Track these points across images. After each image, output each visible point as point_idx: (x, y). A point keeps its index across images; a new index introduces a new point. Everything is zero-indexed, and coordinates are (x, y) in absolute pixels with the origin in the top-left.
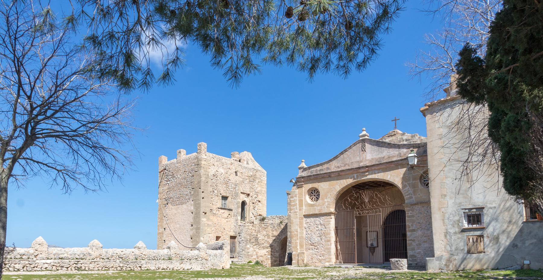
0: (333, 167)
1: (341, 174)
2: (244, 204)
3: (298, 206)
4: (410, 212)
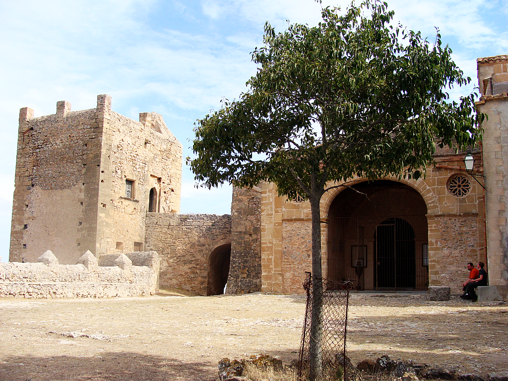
2: (153, 192)
3: (274, 207)
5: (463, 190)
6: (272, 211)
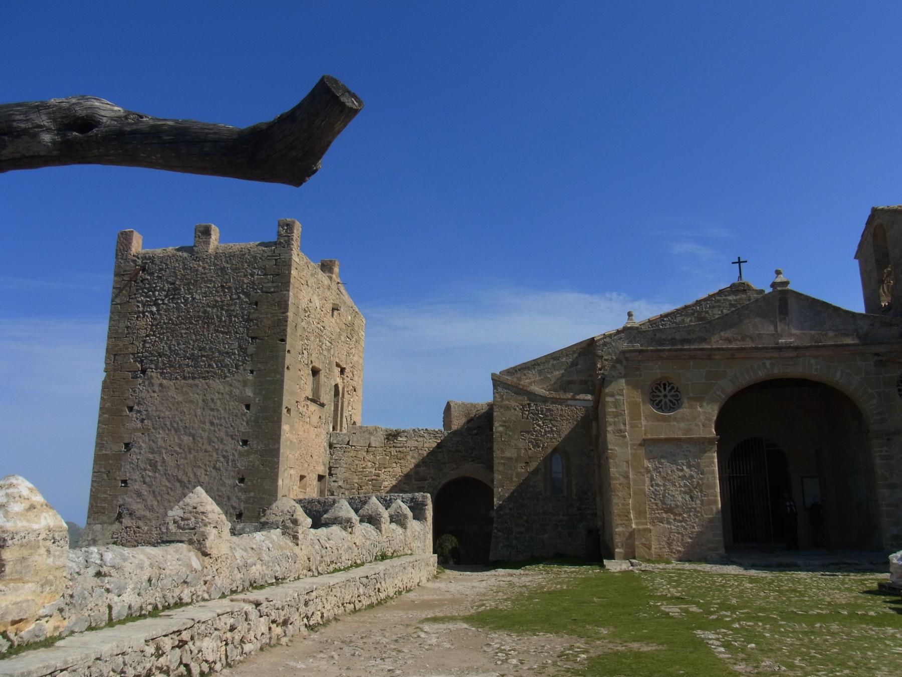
3: (627, 418)
4: (886, 448)
6: (625, 424)
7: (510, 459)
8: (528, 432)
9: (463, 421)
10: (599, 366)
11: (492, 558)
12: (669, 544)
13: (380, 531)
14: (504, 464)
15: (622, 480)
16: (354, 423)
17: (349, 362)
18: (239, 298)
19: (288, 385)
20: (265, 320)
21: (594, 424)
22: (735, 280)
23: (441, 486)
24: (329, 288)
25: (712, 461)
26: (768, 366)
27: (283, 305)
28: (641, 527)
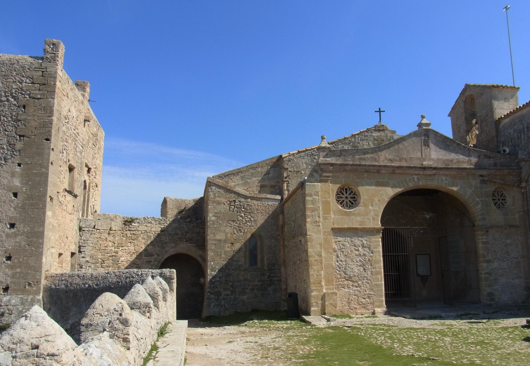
0: (382, 158)
1: (397, 171)
3: (321, 213)
4: (485, 237)
5: (343, 201)
6: (319, 217)
7: (220, 241)
8: (233, 221)
9: (176, 212)
10: (285, 175)
11: (205, 313)
12: (349, 303)
13: (158, 308)
14: (215, 244)
15: (317, 257)
16: (96, 211)
17: (93, 164)
18: (8, 100)
19: (52, 178)
20: (32, 122)
21: (281, 216)
22: (376, 123)
23: (163, 260)
24: (83, 103)
25: (377, 241)
26: (416, 180)
27: (49, 111)
28: (329, 291)
